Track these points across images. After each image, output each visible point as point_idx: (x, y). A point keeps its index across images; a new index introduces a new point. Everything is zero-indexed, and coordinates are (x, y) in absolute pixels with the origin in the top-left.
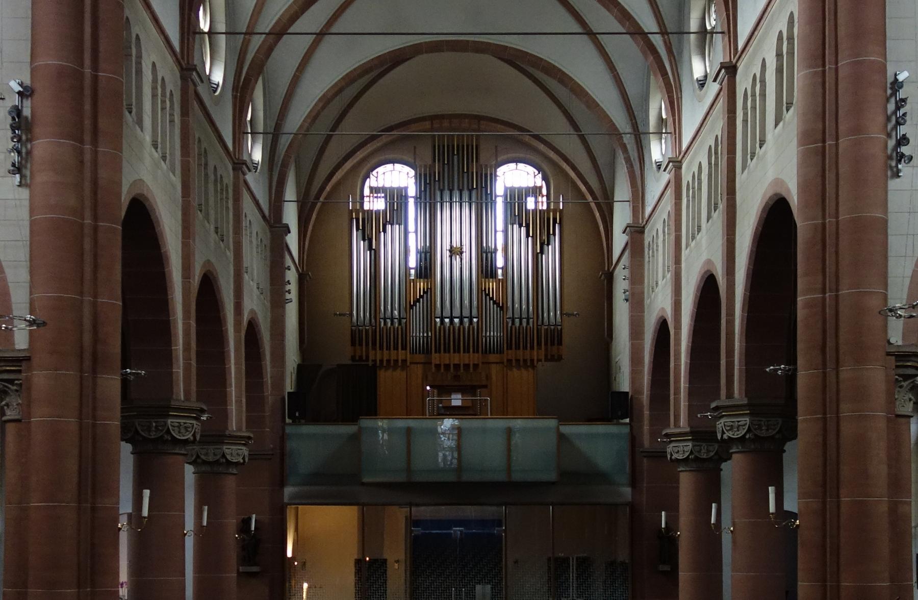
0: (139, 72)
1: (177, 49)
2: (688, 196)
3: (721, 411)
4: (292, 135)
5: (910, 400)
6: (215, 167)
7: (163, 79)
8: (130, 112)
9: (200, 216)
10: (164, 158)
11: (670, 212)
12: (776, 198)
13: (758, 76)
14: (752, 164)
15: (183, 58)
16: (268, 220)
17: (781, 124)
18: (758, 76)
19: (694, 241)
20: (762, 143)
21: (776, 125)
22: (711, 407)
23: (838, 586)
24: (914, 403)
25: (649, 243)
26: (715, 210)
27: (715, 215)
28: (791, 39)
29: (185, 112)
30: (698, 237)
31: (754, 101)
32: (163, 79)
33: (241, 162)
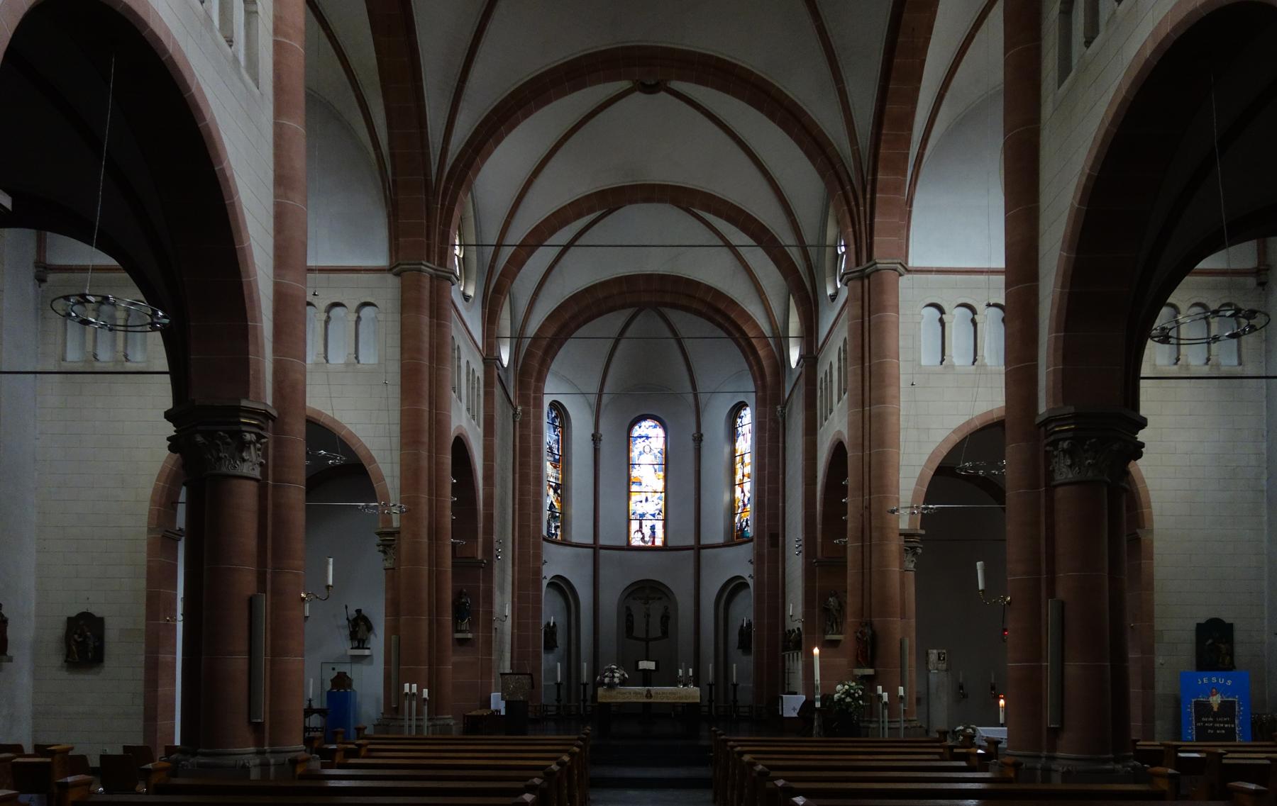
0: (459, 367)
1: (481, 348)
2: (821, 388)
3: (1053, 425)
4: (530, 339)
5: (912, 561)
6: (468, 362)
7: (478, 377)
8: (455, 392)
9: (454, 396)
10: (473, 416)
11: (847, 339)
12: (838, 441)
13: (828, 371)
14: (826, 424)
15: (483, 351)
16: (516, 412)
17: (841, 402)
18: (828, 371)
19: (827, 421)
20: (831, 411)
21: (838, 402)
22: (1036, 423)
23: (430, 665)
24: (915, 563)
25: (822, 379)
26: (825, 420)
27: (845, 397)
28: (845, 351)
29: (489, 395)
30: (830, 417)
31: (826, 385)
32: (478, 377)
33: (450, 271)
